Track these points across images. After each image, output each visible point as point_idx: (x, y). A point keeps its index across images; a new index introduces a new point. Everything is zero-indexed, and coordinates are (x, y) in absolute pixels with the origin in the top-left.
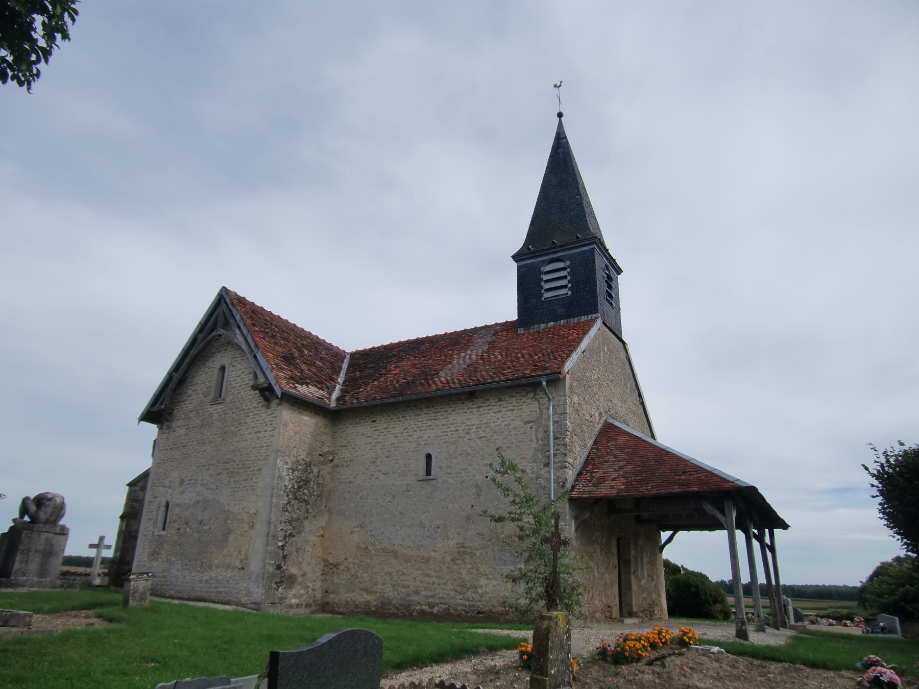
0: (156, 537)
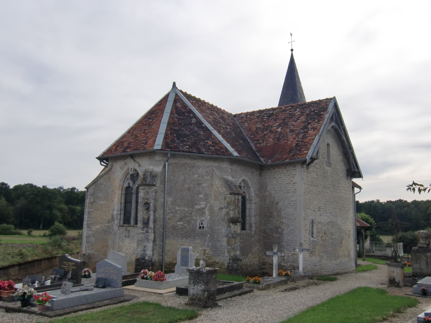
0: (311, 242)
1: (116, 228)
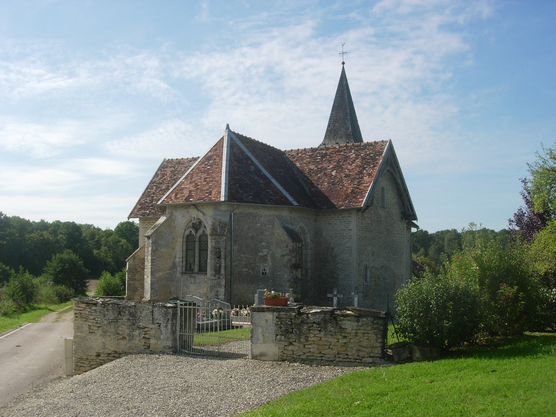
0: (365, 286)
1: (178, 275)
